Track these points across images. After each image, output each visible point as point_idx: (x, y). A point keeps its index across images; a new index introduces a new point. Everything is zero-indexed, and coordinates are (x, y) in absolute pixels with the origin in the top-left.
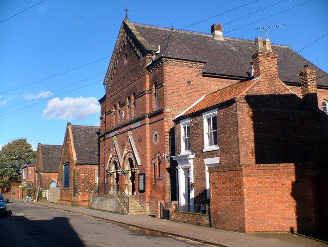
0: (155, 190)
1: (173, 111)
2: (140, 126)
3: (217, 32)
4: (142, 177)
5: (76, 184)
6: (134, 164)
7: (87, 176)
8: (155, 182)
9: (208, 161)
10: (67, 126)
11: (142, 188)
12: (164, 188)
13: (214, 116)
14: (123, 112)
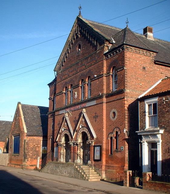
2: (95, 105)
4: (98, 149)
5: (26, 151)
7: (34, 145)
8: (111, 153)
10: (18, 104)
11: (97, 157)
12: (123, 159)
14: (76, 93)
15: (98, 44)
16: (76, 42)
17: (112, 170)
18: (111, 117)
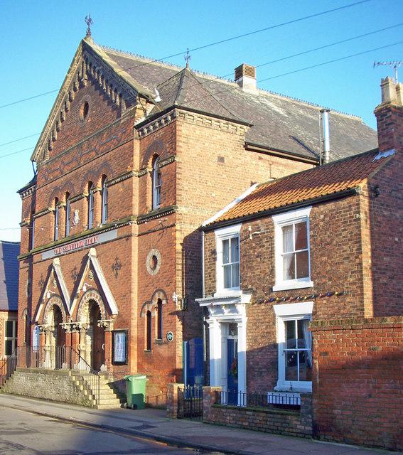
0: (150, 363)
1: (189, 218)
3: (246, 79)
6: (103, 312)
8: (149, 347)
9: (284, 311)
11: (119, 357)
13: (299, 221)
14: (77, 212)
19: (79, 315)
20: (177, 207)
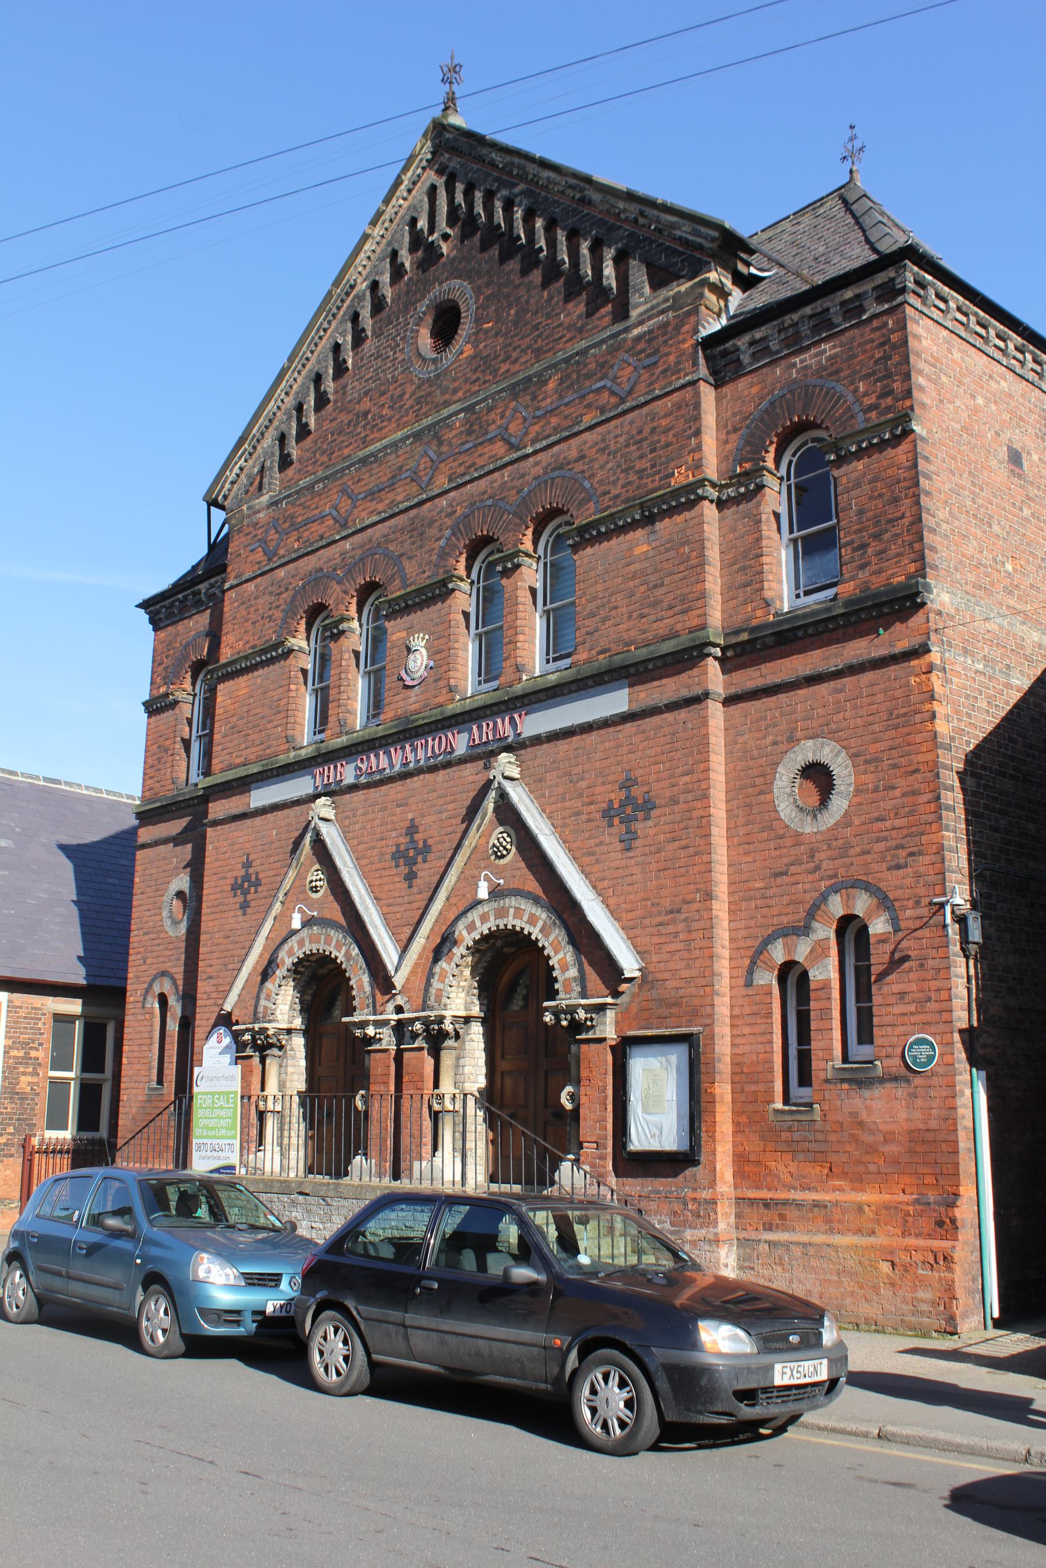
15: (638, 275)
16: (408, 300)
17: (819, 1238)
18: (786, 810)
19: (436, 984)
20: (928, 588)
